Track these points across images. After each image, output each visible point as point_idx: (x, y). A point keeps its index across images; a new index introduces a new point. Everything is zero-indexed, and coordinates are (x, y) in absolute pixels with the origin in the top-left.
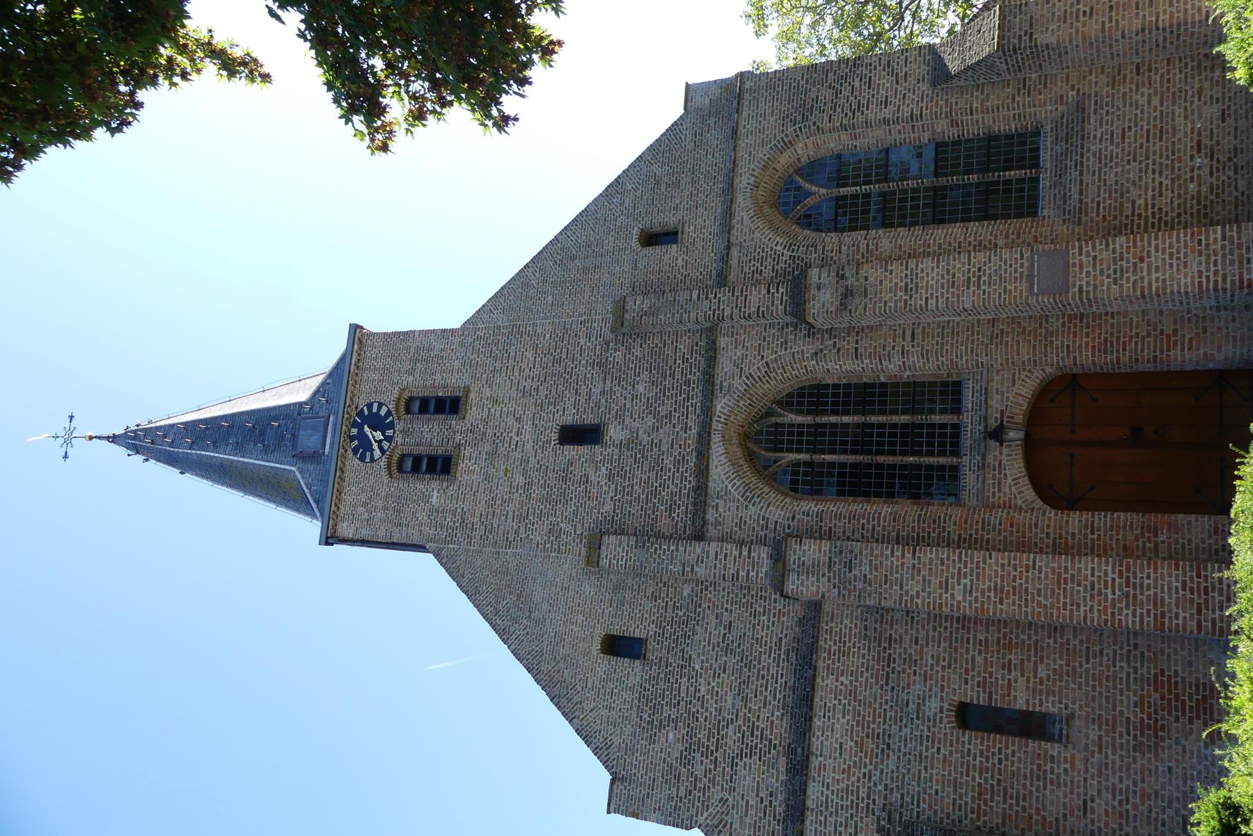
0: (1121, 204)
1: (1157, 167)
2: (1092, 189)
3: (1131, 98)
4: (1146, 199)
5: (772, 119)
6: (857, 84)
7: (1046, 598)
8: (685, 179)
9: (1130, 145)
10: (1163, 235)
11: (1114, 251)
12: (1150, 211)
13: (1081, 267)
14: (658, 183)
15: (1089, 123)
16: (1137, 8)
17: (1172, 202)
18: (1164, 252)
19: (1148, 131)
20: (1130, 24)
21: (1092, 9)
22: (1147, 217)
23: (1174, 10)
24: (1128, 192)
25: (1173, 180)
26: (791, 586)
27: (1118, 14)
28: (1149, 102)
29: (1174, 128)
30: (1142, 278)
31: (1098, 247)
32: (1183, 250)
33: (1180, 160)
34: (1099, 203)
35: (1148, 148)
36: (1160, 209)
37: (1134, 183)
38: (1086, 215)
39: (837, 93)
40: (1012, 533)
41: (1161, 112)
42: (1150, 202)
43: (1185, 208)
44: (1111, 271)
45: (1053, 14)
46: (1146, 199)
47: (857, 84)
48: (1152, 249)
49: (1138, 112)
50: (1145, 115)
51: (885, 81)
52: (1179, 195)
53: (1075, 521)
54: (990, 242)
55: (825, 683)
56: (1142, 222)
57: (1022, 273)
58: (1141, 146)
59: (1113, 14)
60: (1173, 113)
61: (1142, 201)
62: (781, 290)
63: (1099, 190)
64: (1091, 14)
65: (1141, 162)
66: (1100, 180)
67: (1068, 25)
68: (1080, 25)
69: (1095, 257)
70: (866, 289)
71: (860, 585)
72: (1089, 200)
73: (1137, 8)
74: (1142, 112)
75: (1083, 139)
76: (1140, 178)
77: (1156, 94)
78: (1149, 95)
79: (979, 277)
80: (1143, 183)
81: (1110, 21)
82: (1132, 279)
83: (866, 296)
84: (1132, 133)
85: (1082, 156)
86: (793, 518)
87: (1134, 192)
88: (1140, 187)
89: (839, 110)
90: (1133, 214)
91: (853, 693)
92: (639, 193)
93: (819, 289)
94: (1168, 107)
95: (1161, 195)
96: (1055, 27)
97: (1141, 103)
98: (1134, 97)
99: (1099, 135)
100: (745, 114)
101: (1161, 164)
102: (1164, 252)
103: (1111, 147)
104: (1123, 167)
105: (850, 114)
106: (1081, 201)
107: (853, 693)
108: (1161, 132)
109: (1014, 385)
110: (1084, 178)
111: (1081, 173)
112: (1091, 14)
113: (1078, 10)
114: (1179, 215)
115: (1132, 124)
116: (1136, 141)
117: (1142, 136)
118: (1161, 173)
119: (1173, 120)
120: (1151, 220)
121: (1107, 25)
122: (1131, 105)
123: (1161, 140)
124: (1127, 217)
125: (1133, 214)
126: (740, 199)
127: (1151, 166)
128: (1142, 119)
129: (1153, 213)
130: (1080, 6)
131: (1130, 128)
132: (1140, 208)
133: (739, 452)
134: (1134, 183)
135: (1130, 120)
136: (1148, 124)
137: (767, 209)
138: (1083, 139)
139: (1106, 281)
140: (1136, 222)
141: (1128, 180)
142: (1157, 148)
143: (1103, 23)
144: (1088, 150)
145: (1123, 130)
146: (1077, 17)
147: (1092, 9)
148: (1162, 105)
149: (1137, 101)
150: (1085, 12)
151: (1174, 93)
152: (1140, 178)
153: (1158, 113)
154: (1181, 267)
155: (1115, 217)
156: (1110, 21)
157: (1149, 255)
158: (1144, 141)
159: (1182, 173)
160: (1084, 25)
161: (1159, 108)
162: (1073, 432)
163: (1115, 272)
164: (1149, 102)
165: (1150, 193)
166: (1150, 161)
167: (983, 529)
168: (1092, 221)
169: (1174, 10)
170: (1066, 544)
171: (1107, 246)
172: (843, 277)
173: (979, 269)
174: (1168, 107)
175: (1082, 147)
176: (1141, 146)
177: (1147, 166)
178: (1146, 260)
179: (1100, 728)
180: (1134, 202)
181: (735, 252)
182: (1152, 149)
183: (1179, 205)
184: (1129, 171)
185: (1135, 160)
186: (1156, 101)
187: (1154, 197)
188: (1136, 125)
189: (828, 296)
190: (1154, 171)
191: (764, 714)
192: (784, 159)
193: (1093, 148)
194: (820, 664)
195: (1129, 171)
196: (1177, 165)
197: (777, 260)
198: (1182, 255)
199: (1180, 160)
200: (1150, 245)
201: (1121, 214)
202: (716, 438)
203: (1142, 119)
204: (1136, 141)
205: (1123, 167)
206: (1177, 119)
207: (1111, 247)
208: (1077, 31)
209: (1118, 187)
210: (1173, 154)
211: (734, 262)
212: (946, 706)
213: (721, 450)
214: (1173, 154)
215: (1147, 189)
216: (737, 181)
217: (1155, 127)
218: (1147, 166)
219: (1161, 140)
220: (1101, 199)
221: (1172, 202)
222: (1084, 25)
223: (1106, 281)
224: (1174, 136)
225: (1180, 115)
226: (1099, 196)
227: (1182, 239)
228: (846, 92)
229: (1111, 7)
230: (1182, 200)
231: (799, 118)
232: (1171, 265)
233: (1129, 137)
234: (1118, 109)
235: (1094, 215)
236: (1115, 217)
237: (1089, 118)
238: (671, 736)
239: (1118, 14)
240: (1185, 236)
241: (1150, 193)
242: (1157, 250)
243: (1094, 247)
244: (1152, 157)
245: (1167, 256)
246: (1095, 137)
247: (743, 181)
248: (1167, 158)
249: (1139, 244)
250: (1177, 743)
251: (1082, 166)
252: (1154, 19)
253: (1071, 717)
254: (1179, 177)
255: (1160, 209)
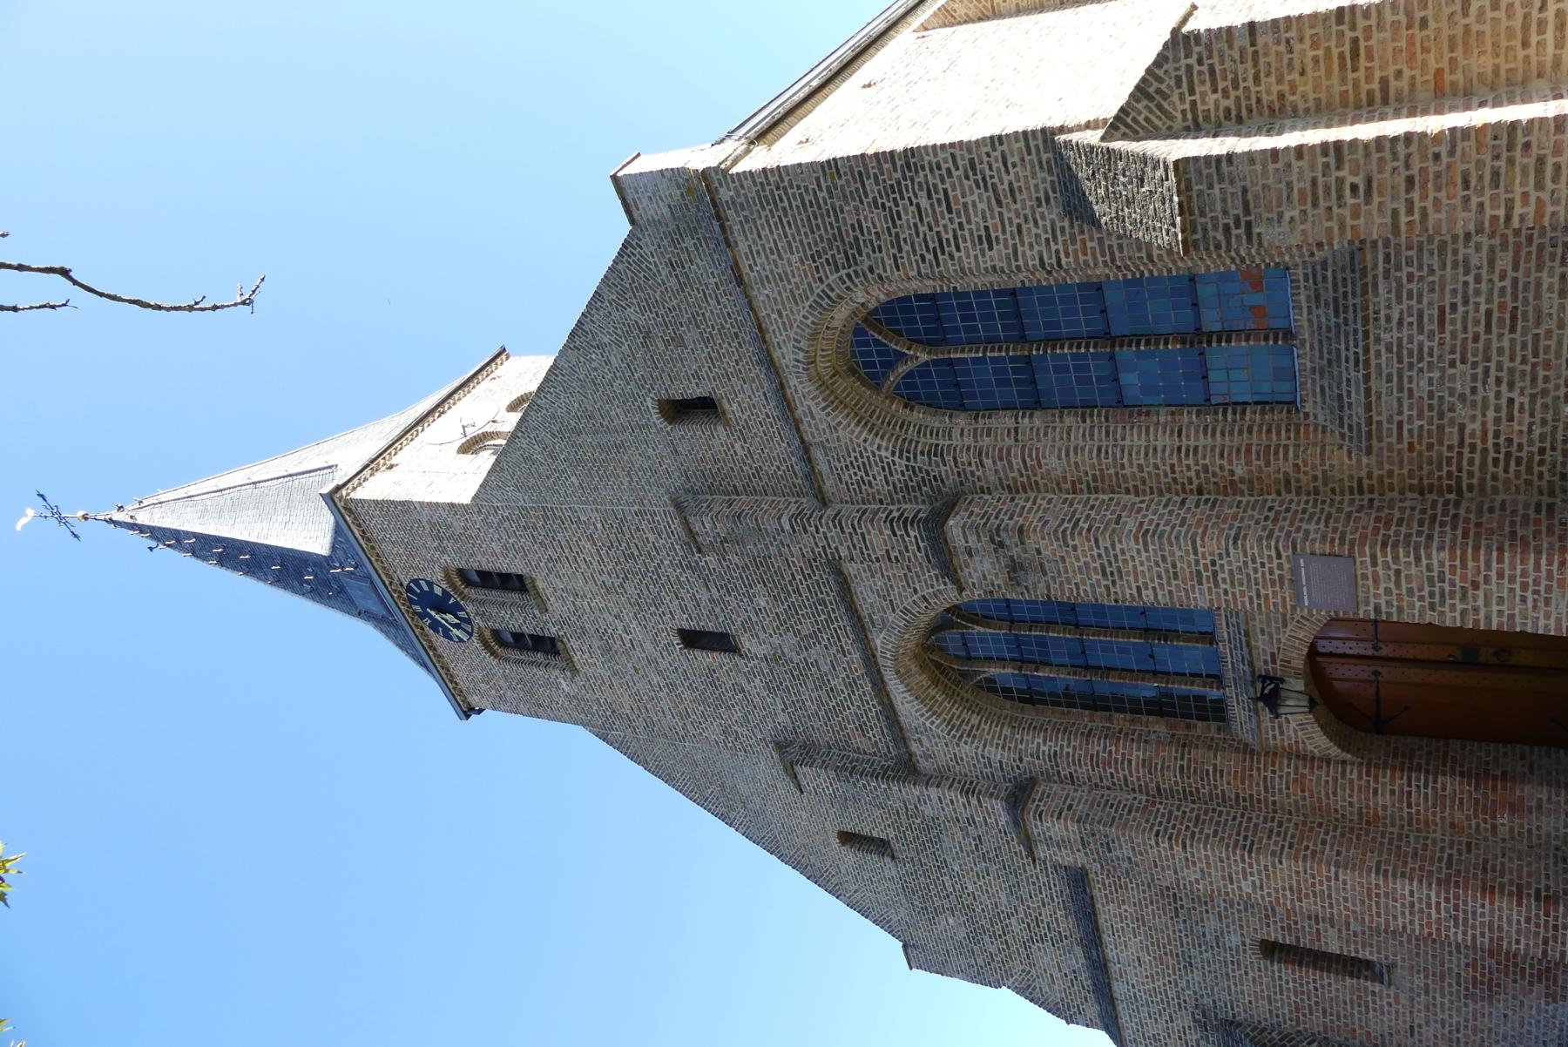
0: (1441, 428)
1: (1504, 374)
2: (1388, 404)
3: (1455, 252)
4: (1484, 424)
5: (795, 258)
6: (924, 203)
7: (1354, 904)
8: (691, 336)
9: (1454, 335)
10: (1513, 557)
11: (1429, 568)
12: (1491, 441)
13: (1376, 581)
14: (648, 335)
15: (1376, 295)
16: (1466, 184)
17: (1530, 431)
18: (1512, 579)
19: (1489, 313)
20: (1452, 222)
21: (1369, 181)
22: (1485, 450)
23: (1545, 196)
24: (1452, 410)
25: (1533, 397)
26: (1042, 851)
27: (1424, 197)
28: (1491, 263)
29: (1538, 311)
30: (1476, 610)
31: (1403, 559)
32: (1544, 583)
33: (1547, 365)
34: (1400, 424)
35: (1488, 343)
36: (1509, 441)
37: (1463, 398)
38: (1380, 440)
39: (894, 217)
40: (1304, 798)
41: (1515, 281)
42: (1491, 428)
43: (1554, 440)
44: (1425, 593)
45: (1289, 185)
46: (1484, 424)
47: (924, 203)
48: (1493, 574)
49: (1470, 279)
50: (1484, 286)
51: (977, 199)
52: (1544, 422)
53: (1386, 792)
54: (1222, 467)
55: (1107, 913)
56: (1477, 457)
57: (1281, 577)
58: (1476, 339)
59: (1416, 195)
60: (1538, 285)
61: (1477, 426)
62: (912, 533)
63: (1400, 405)
64: (1368, 192)
65: (1475, 365)
66: (1400, 390)
67: (1321, 210)
68: (1346, 212)
69: (1398, 573)
70: (1042, 565)
71: (1126, 864)
72: (1383, 418)
73: (1466, 184)
74: (1478, 280)
75: (1366, 320)
76: (1474, 390)
77: (1504, 246)
78: (1492, 249)
79: (1215, 574)
80: (1479, 398)
81: (1410, 211)
82: (1459, 607)
83: (1045, 574)
84: (1458, 316)
85: (1366, 350)
86: (1021, 760)
87: (1462, 412)
88: (1474, 405)
89: (906, 248)
90: (1461, 444)
91: (1141, 920)
92: (625, 348)
93: (970, 555)
94: (1528, 273)
95: (1511, 419)
96: (1296, 213)
97: (1474, 261)
98: (1462, 251)
99: (1396, 317)
100: (743, 247)
101: (1512, 371)
102: (1512, 579)
103: (1417, 338)
104: (1443, 370)
105: (930, 257)
106: (1369, 421)
107: (1141, 920)
108: (1514, 318)
109: (1285, 626)
110: (1374, 385)
111: (1367, 378)
112: (1368, 192)
113: (1340, 181)
114: (1542, 451)
115: (1459, 299)
116: (1465, 329)
117: (1477, 322)
118: (1511, 386)
119: (1538, 296)
120: (1492, 454)
121: (1404, 219)
122: (1455, 265)
123: (1513, 330)
124: (1450, 448)
125: (1461, 444)
126: (793, 382)
127: (1493, 373)
128: (1477, 292)
129: (1496, 445)
130: (1344, 173)
131: (1454, 306)
132: (1473, 435)
133: (923, 679)
134: (1463, 398)
135: (1454, 292)
136: (1489, 301)
137: (845, 384)
138: (1366, 320)
139: (1418, 604)
140: (1466, 455)
141: (1452, 392)
142: (1506, 343)
143: (1395, 212)
144: (1378, 340)
145: (1442, 310)
146: (1340, 197)
147: (1369, 181)
148: (1516, 268)
149: (1466, 261)
150: (1354, 188)
151: (1541, 248)
152: (1474, 390)
153: (1507, 283)
154: (1541, 604)
155: (1430, 447)
156: (1410, 211)
157: (1487, 579)
158: (1482, 329)
159: (1551, 386)
160: (1356, 215)
161: (1510, 274)
162: (1376, 648)
163: (1432, 595)
164: (1491, 263)
165: (1491, 414)
166: (1493, 365)
167: (1266, 791)
168: (1390, 449)
169: (1545, 196)
170: (1376, 815)
171: (1418, 559)
172: (1001, 545)
173: (1213, 563)
174: (1528, 273)
175: (1366, 334)
176: (1476, 339)
177: (1486, 372)
178: (1483, 587)
179: (1426, 977)
180: (1462, 427)
181: (818, 454)
182: (1495, 345)
183: (1542, 437)
184: (1453, 378)
185: (1463, 362)
186: (1504, 261)
187: (1497, 421)
188: (1466, 303)
189: (987, 566)
190: (1499, 381)
191: (1045, 912)
192: (841, 314)
193: (1385, 337)
194: (1096, 893)
195: (1453, 378)
196: (1541, 373)
197: (888, 468)
198: (1542, 588)
199: (1547, 365)
200: (1488, 567)
201: (1441, 442)
202: (889, 675)
203: (1477, 292)
204: (1465, 329)
205: (1443, 370)
206: (1546, 295)
207: (1424, 562)
208: (1342, 226)
209: (1435, 402)
210: (1536, 355)
211: (823, 467)
212: (1248, 941)
213: (902, 688)
214: (1536, 355)
215: (1485, 407)
216: (776, 354)
217: (1502, 306)
218: (1486, 372)
219: (1513, 330)
220: (1405, 418)
221: (1530, 431)
222: (1356, 215)
223: (1418, 604)
224: (1538, 324)
225: (1550, 289)
226: (1400, 413)
227: (1544, 568)
228: (909, 216)
229: (1410, 181)
230: (1548, 429)
231: (840, 259)
232: (1524, 599)
233: (1453, 322)
234: (1432, 271)
235: (1394, 440)
236: (1430, 447)
237: (1375, 285)
238: (951, 921)
239: (1424, 197)
240: (1550, 563)
241: (1491, 414)
242: (1500, 575)
243: (1396, 559)
244: (1495, 358)
245: (1517, 587)
246: (1388, 319)
247: (786, 356)
248: (1524, 361)
249: (1470, 564)
250: (1514, 997)
251: (1367, 363)
252: (1501, 213)
253: (1394, 965)
254: (1545, 392)
255: (1509, 441)
